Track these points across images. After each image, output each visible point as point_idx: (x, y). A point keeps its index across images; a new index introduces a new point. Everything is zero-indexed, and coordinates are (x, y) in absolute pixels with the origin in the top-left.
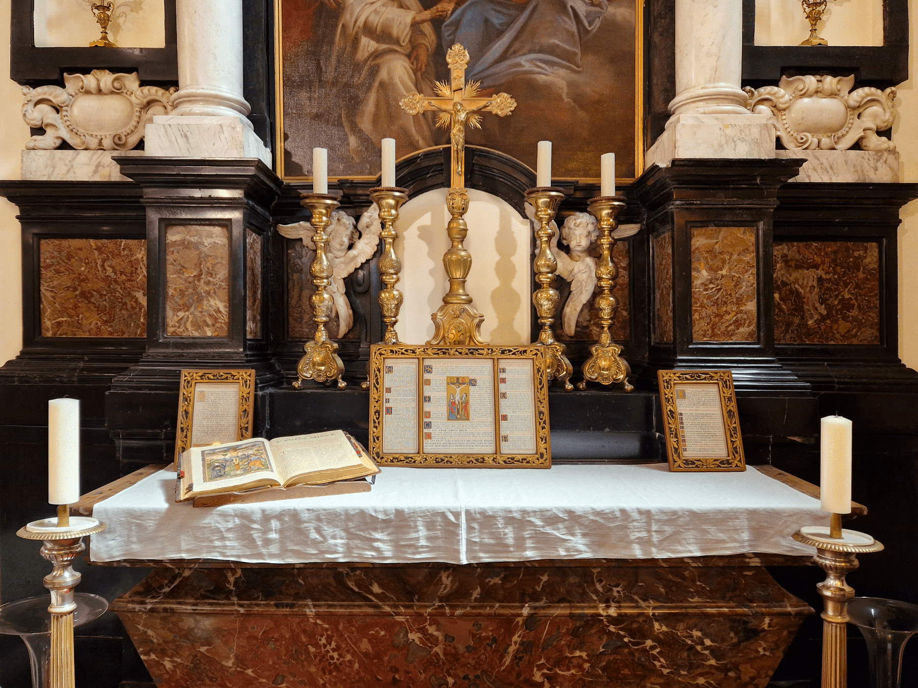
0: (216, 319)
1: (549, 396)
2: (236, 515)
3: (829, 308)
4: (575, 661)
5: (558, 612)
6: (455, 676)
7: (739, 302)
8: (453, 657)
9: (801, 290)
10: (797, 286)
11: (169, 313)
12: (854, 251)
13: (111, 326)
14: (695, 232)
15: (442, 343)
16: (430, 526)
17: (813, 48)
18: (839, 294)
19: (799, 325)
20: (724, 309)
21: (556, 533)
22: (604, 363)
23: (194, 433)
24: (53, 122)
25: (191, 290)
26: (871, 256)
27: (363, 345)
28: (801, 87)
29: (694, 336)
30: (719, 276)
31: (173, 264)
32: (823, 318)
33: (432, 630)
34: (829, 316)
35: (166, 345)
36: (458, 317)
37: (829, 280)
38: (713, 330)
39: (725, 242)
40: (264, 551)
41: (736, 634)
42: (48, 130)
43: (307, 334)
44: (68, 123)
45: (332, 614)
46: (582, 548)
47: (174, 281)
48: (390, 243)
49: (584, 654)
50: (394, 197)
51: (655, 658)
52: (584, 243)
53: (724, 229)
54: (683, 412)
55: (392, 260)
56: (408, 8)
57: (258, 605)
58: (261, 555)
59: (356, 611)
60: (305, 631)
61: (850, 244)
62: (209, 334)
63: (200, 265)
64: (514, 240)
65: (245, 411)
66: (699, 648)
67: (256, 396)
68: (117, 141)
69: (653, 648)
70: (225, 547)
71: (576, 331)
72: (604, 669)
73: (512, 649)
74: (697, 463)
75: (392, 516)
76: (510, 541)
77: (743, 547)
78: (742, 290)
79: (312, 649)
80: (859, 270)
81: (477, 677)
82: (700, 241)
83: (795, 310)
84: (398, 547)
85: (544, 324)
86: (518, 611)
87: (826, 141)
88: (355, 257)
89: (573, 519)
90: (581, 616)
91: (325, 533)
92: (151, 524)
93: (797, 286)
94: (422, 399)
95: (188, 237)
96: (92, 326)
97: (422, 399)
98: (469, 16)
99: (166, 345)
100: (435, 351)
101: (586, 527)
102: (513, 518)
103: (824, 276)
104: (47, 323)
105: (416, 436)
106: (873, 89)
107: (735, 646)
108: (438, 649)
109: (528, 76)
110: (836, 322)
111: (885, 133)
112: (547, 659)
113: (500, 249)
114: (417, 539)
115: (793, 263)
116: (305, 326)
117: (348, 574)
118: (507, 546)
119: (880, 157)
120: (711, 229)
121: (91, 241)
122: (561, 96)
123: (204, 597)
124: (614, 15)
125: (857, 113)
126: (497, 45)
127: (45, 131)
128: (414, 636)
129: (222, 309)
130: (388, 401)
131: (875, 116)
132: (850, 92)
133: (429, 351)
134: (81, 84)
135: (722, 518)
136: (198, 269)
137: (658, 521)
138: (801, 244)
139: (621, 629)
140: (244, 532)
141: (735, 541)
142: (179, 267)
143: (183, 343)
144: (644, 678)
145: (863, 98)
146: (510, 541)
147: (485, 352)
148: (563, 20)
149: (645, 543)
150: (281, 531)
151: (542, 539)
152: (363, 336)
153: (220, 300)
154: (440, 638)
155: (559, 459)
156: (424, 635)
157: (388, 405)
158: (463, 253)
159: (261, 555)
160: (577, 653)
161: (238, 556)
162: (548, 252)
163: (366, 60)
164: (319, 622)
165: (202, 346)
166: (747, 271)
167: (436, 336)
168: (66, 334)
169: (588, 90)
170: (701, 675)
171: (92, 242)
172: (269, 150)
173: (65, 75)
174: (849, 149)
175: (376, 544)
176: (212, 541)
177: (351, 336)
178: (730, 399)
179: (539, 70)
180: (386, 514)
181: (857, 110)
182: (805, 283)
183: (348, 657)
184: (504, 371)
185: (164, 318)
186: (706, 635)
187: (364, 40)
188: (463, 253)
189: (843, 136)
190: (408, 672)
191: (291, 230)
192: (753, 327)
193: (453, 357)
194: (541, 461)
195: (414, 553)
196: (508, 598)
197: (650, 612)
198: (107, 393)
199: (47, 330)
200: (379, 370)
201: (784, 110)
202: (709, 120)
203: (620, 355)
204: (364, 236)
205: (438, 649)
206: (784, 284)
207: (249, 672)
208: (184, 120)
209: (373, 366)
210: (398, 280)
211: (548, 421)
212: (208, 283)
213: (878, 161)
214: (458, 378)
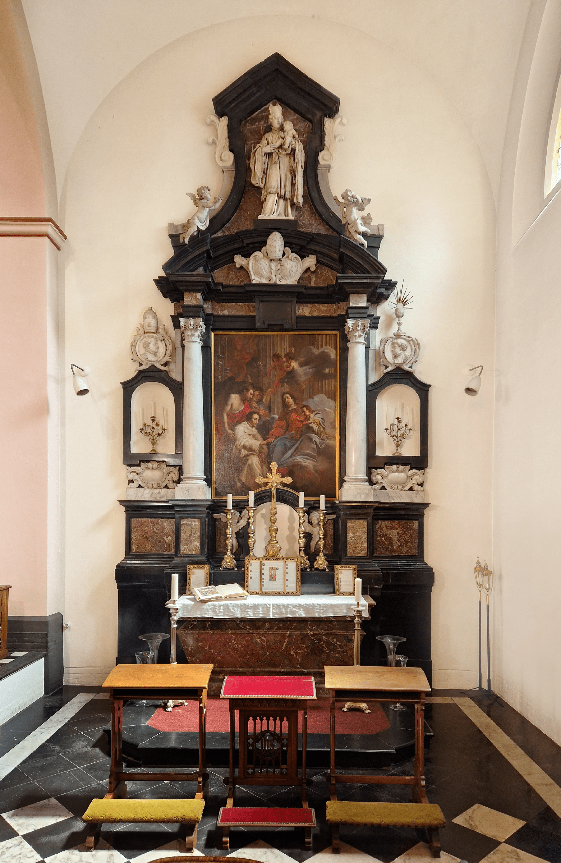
0: (196, 548)
3: (401, 543)
4: (302, 648)
6: (269, 652)
8: (269, 646)
9: (391, 537)
11: (181, 546)
14: (348, 521)
15: (268, 556)
16: (263, 608)
19: (390, 549)
23: (192, 584)
25: (188, 539)
26: (416, 524)
27: (242, 556)
32: (399, 546)
33: (263, 638)
34: (401, 546)
40: (219, 615)
41: (345, 640)
42: (135, 481)
44: (142, 479)
45: (236, 633)
46: (303, 614)
47: (183, 536)
49: (305, 646)
50: (253, 510)
51: (324, 647)
53: (357, 521)
56: (258, 440)
57: (216, 631)
59: (242, 632)
60: (228, 638)
61: (408, 521)
62: (194, 553)
66: (336, 645)
68: (159, 486)
69: (323, 644)
70: (209, 613)
71: (315, 550)
72: (310, 651)
73: (285, 644)
75: (253, 605)
76: (284, 612)
79: (230, 644)
80: (411, 530)
82: (349, 524)
84: (254, 613)
87: (400, 487)
88: (239, 526)
89: (300, 606)
92: (190, 608)
94: (261, 574)
97: (261, 574)
98: (279, 443)
103: (399, 532)
104: (133, 547)
107: (346, 645)
108: (265, 644)
109: (300, 463)
110: (404, 547)
111: (421, 485)
112: (295, 647)
115: (389, 528)
116: (221, 548)
119: (418, 493)
120: (353, 521)
125: (411, 478)
128: (257, 640)
130: (251, 575)
131: (416, 479)
134: (146, 466)
135: (339, 606)
140: (214, 609)
141: (342, 612)
144: (322, 654)
145: (412, 473)
146: (284, 612)
149: (319, 612)
150: (223, 609)
151: (292, 612)
153: (198, 542)
160: (303, 646)
162: (303, 527)
163: (244, 457)
168: (140, 551)
170: (337, 653)
173: (141, 463)
174: (408, 490)
175: (248, 613)
177: (237, 552)
178: (355, 574)
179: (303, 461)
180: (251, 605)
181: (411, 477)
183: (240, 646)
185: (180, 548)
187: (243, 450)
189: (406, 485)
192: (366, 551)
195: (258, 615)
196: (284, 629)
197: (322, 633)
198: (164, 572)
199: (134, 550)
202: (352, 487)
205: (265, 644)
206: (386, 535)
207: (212, 651)
209: (246, 564)
213: (417, 494)
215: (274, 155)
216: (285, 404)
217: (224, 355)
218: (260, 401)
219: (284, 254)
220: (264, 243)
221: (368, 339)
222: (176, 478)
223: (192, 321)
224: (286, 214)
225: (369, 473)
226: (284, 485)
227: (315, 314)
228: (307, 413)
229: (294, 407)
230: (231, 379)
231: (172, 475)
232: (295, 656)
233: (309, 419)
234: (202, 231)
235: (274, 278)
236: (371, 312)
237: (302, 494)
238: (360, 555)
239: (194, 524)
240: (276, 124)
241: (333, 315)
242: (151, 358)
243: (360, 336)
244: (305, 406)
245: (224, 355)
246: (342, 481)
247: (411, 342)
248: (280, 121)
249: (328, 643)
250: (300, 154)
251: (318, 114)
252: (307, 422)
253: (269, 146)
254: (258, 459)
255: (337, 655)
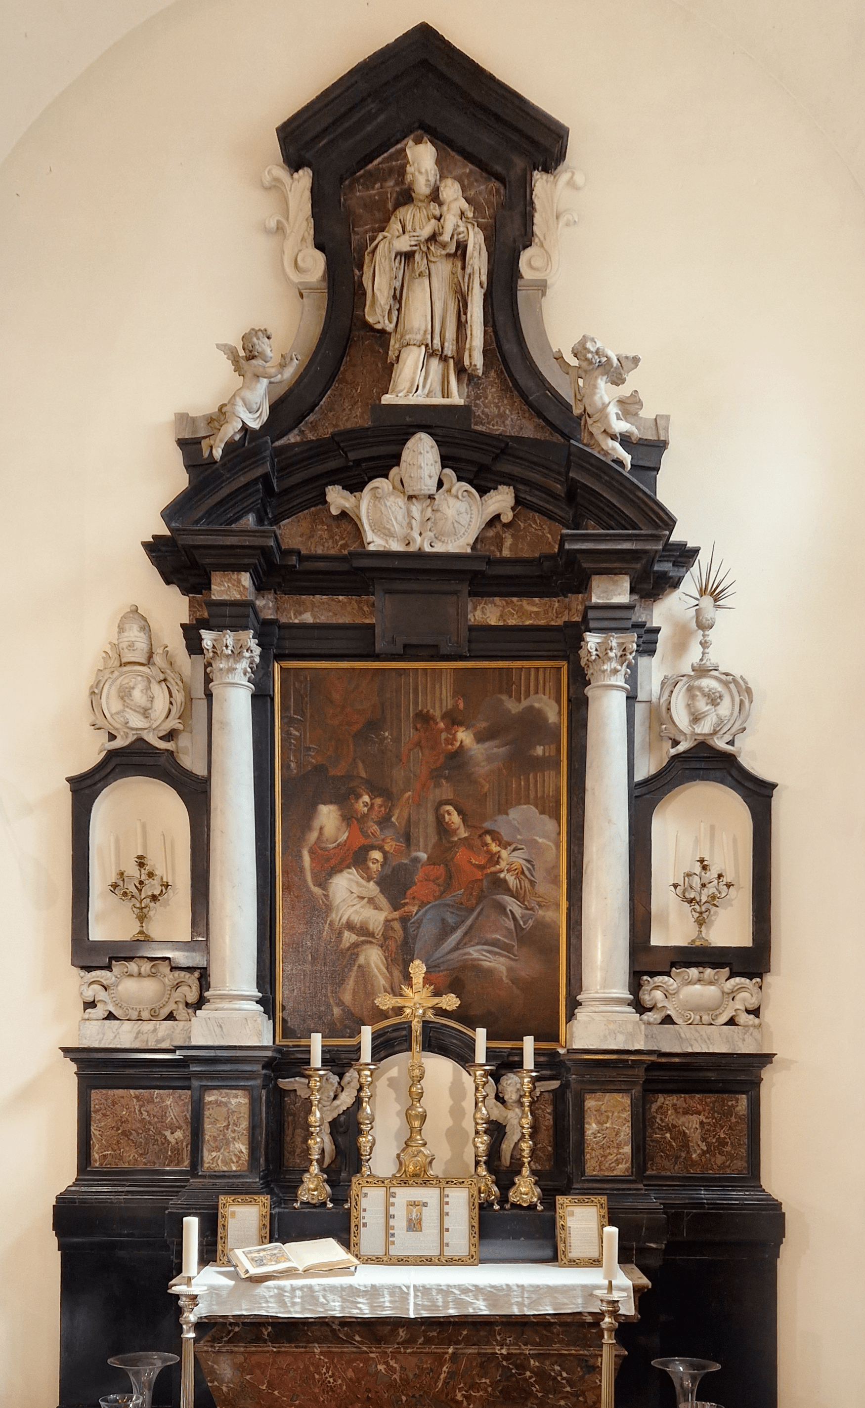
0: (239, 1158)
1: (479, 1214)
2: (275, 1288)
3: (709, 1145)
5: (470, 1351)
7: (619, 1146)
8: (406, 1381)
9: (687, 1131)
10: (684, 1128)
11: (206, 1153)
12: (728, 1101)
13: (145, 1158)
14: (587, 1096)
15: (404, 1176)
16: (392, 1294)
17: (697, 947)
18: (716, 1134)
19: (685, 1158)
20: (608, 1151)
21: (467, 1298)
22: (523, 1190)
24: (104, 999)
25: (221, 1137)
26: (742, 1103)
27: (344, 1175)
28: (686, 977)
29: (587, 1171)
30: (604, 1128)
31: (208, 1118)
32: (704, 1153)
33: (392, 1363)
34: (708, 1151)
35: (204, 1177)
36: (416, 1156)
37: (709, 1124)
38: (600, 1166)
39: (609, 1103)
40: (292, 1309)
42: (99, 1005)
43: (299, 1164)
44: (114, 999)
45: (331, 1352)
47: (210, 1130)
48: (366, 1102)
49: (488, 1381)
50: (370, 1070)
51: (533, 1385)
52: (515, 1097)
54: (571, 1226)
55: (367, 1114)
56: (382, 910)
58: (290, 1312)
60: (313, 1364)
61: (725, 1096)
62: (234, 1168)
63: (229, 1117)
64: (464, 1088)
65: (264, 1225)
67: (271, 1214)
68: (153, 1013)
69: (531, 1377)
70: (268, 1307)
71: (511, 1162)
72: (501, 1392)
73: (443, 1376)
74: (577, 1261)
75: (369, 1289)
76: (440, 1303)
77: (579, 1308)
78: (620, 1139)
79: (317, 1376)
80: (731, 1116)
81: (421, 1396)
83: (683, 1147)
84: (372, 1307)
85: (480, 1161)
86: (446, 1350)
87: (706, 1018)
89: (478, 1290)
90: (486, 1354)
91: (328, 1298)
92: (224, 1293)
93: (684, 1128)
94: (389, 1216)
95: (220, 1098)
96: (131, 1158)
97: (389, 1216)
98: (429, 916)
99: (204, 1177)
100: (398, 1182)
101: (486, 1295)
102: (442, 1289)
104: (96, 1156)
105: (384, 1243)
106: (743, 979)
108: (396, 1376)
109: (476, 963)
110: (715, 1156)
111: (755, 1012)
112: (465, 1384)
113: (452, 1095)
114: (384, 1302)
115: (681, 1110)
116: (297, 1157)
117: (339, 1330)
118: (439, 1307)
119: (747, 1031)
120: (599, 1095)
121: (131, 1091)
122: (501, 979)
123: (250, 1342)
124: (544, 917)
126: (453, 937)
127: (96, 1006)
128: (381, 1367)
129: (244, 1150)
130: (364, 1218)
132: (726, 980)
133: (394, 1182)
134: (126, 970)
135: (566, 1290)
136: (227, 1122)
137: (528, 1291)
138: (687, 1096)
139: (510, 1364)
142: (213, 1120)
143: (215, 1175)
144: (526, 1399)
145: (735, 986)
146: (440, 1303)
147: (434, 1183)
148: (504, 920)
149: (520, 1305)
151: (459, 1303)
152: (343, 1168)
153: (242, 1144)
154: (398, 1368)
155: (482, 1261)
156: (387, 1366)
157: (364, 1221)
158: (420, 1110)
159: (290, 1312)
160: (484, 1380)
161: (276, 1313)
162: (483, 1109)
163: (349, 949)
164: (322, 1357)
165: (229, 1177)
166: (624, 1124)
167: (399, 1171)
169: (523, 974)
171: (132, 1091)
172: (271, 1021)
173: (114, 962)
176: (260, 1303)
177: (333, 1166)
178: (604, 1217)
179: (484, 958)
180: (366, 1287)
181: (732, 995)
182: (690, 1126)
183: (340, 1382)
184: (448, 1196)
185: (202, 1157)
186: (563, 1369)
187: (346, 934)
188: (420, 1110)
189: (721, 1014)
190: (377, 1392)
191: (285, 1083)
192: (629, 1165)
193: (412, 1186)
194: (472, 1260)
195: (382, 1311)
196: (441, 1343)
199: (96, 1161)
200: (358, 1196)
201: (674, 994)
203: (534, 1184)
204: (345, 1089)
205: (396, 1376)
206: (674, 1126)
207: (276, 1393)
208: (217, 1014)
210: (372, 1128)
211: (477, 1233)
212: (234, 1131)
213: (745, 1034)
214: (415, 1202)
215: (417, 257)
216: (443, 829)
217: (303, 715)
218: (384, 822)
219: (440, 484)
220: (395, 459)
221: (632, 679)
222: (192, 997)
223: (229, 638)
224: (446, 393)
225: (635, 986)
226: (440, 1012)
227: (512, 622)
228: (494, 848)
229: (463, 833)
230: (320, 769)
231: (184, 989)
232: (465, 1403)
233: (498, 863)
234: (254, 431)
235: (419, 539)
236: (639, 616)
237: (481, 1034)
238: (615, 1173)
239: (234, 1101)
240: (422, 188)
241: (553, 623)
242: (137, 721)
243: (615, 671)
244: (488, 832)
245: (303, 715)
246: (574, 1005)
247: (732, 686)
248: (432, 179)
249: (541, 1374)
250: (476, 254)
251: (519, 163)
252: (493, 869)
253: (406, 236)
254: (380, 952)
255: (562, 1403)
